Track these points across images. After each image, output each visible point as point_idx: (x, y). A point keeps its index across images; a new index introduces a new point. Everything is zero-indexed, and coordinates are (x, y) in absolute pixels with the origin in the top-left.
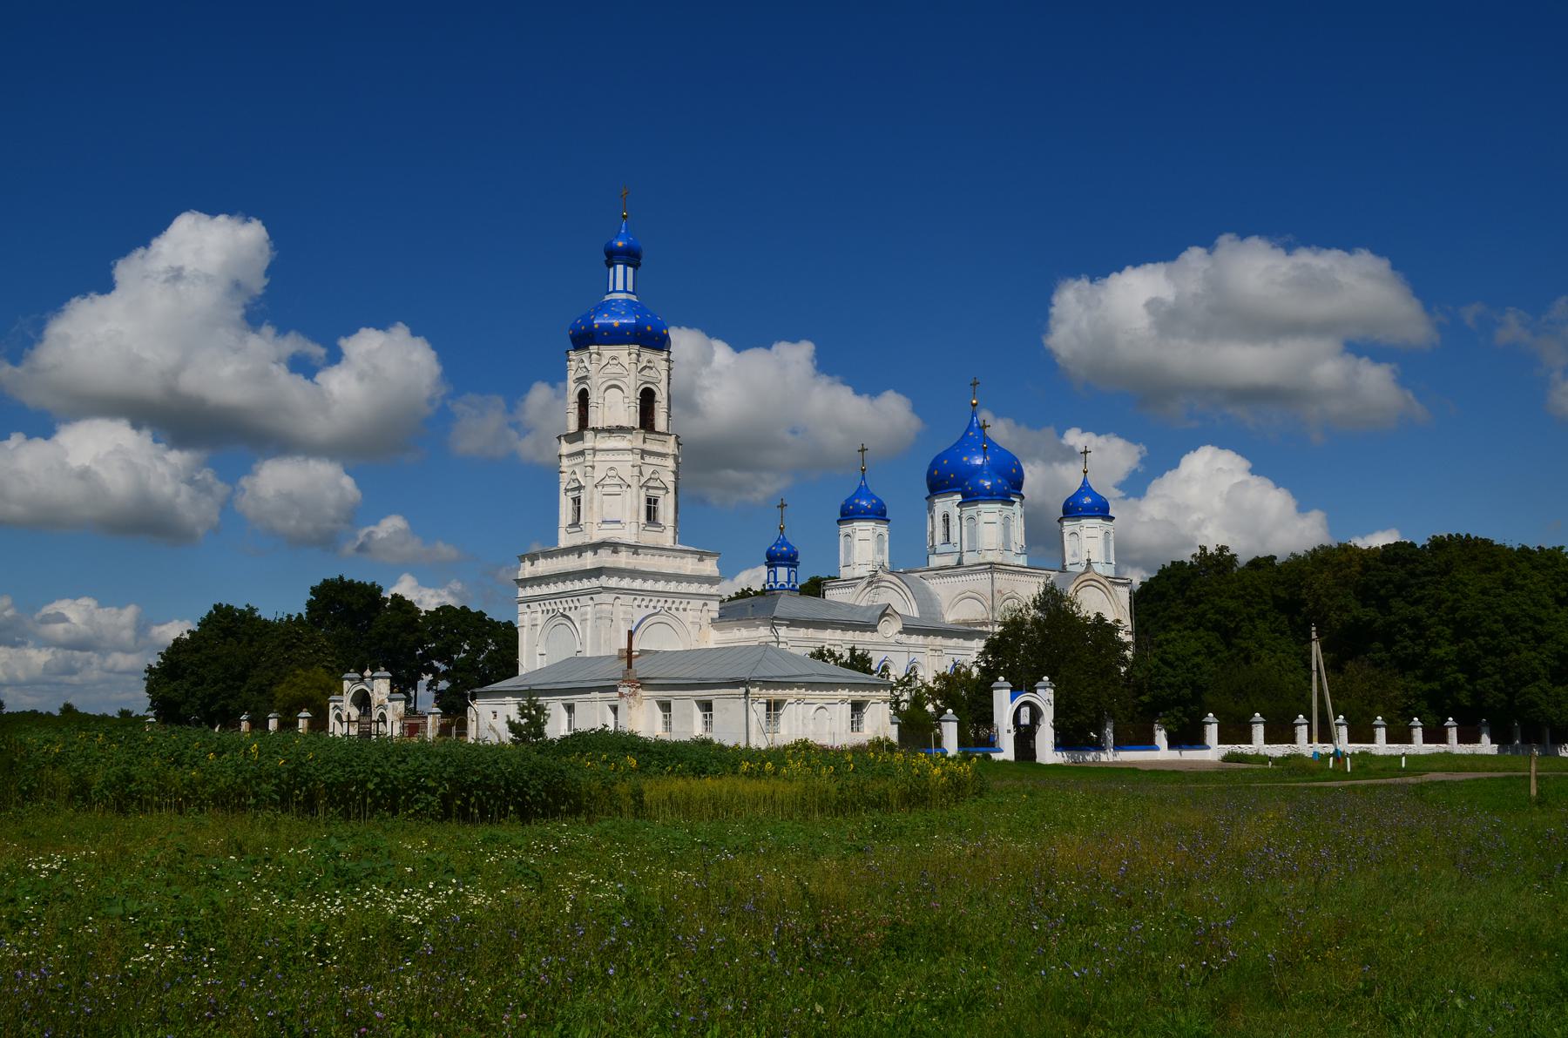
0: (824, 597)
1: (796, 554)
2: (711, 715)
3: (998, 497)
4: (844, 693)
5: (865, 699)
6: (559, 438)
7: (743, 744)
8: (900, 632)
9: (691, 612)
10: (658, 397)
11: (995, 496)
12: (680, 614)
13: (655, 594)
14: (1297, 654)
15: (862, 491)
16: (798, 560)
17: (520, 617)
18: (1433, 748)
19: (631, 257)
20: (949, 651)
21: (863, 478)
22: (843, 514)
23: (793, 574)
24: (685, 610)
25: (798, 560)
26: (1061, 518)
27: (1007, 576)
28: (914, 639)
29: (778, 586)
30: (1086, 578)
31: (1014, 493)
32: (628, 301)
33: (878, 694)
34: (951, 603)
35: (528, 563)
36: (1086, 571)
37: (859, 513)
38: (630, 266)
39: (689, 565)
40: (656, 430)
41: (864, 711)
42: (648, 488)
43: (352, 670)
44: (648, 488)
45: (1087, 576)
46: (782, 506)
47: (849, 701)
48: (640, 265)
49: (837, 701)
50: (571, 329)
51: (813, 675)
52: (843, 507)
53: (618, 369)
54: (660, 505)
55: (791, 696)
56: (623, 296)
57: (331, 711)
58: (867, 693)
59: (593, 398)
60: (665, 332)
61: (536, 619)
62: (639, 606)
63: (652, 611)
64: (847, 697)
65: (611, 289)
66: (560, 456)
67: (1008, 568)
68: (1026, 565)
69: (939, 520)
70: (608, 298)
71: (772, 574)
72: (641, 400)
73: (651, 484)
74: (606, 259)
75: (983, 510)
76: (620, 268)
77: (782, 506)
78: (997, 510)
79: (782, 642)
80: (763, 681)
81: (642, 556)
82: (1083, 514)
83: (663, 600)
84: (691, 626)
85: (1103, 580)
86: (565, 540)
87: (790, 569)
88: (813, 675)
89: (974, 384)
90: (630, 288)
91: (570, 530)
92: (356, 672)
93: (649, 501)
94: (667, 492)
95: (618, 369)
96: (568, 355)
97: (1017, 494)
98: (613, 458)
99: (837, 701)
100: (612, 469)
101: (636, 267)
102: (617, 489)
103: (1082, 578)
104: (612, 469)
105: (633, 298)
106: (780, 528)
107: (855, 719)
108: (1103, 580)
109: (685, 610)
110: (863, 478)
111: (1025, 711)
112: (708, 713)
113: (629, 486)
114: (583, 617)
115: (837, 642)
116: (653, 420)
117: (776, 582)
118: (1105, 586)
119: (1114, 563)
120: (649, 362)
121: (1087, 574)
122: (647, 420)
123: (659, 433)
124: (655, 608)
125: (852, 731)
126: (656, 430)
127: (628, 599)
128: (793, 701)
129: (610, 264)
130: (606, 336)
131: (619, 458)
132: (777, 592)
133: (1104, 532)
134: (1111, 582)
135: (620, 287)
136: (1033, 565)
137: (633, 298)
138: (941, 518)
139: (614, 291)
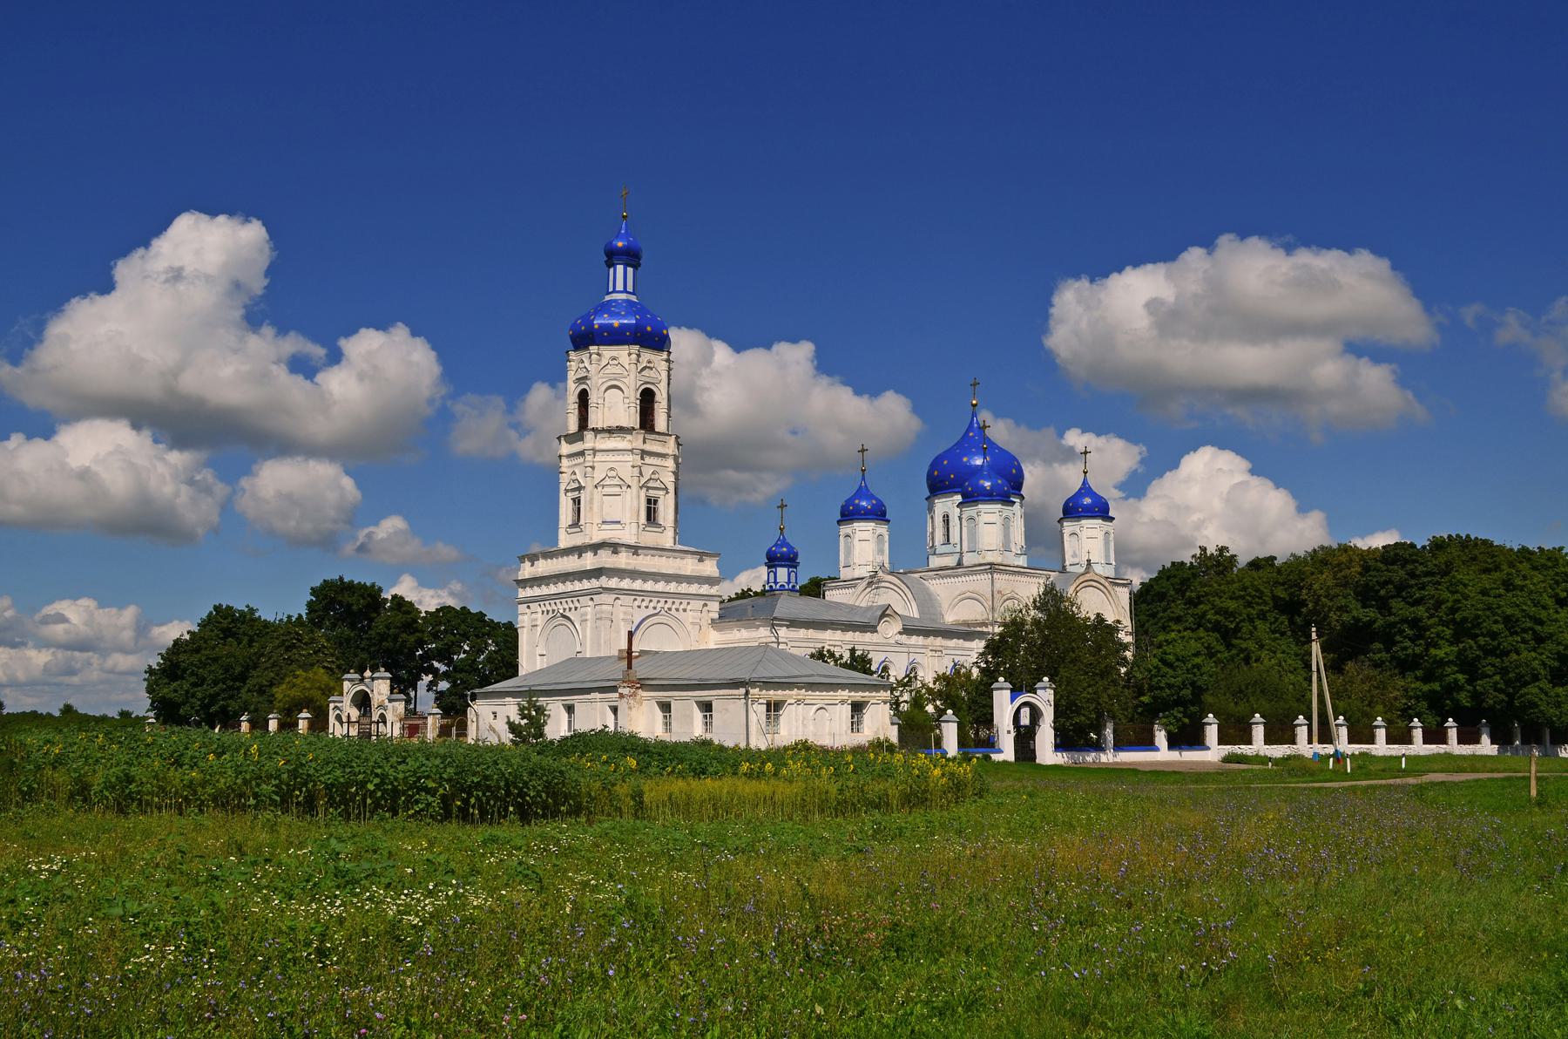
1: (796, 555)
2: (711, 716)
5: (863, 699)
6: (559, 438)
7: (743, 745)
9: (691, 613)
10: (658, 398)
12: (680, 615)
15: (862, 492)
17: (520, 617)
19: (631, 257)
20: (949, 652)
22: (843, 514)
24: (685, 610)
26: (1061, 519)
29: (778, 587)
30: (1086, 579)
32: (628, 301)
33: (879, 694)
35: (528, 564)
36: (1086, 572)
39: (689, 566)
40: (656, 430)
41: (864, 711)
43: (352, 671)
44: (648, 488)
45: (1087, 577)
47: (849, 702)
48: (640, 265)
49: (837, 702)
53: (618, 370)
54: (661, 505)
55: (791, 697)
56: (623, 296)
57: (331, 712)
59: (593, 398)
60: (665, 332)
61: (536, 620)
62: (639, 607)
63: (651, 611)
64: (847, 698)
65: (611, 289)
66: (560, 456)
68: (1026, 566)
70: (608, 298)
73: (651, 484)
76: (620, 268)
77: (782, 507)
78: (997, 511)
80: (763, 682)
82: (1083, 514)
83: (663, 600)
85: (1103, 581)
87: (791, 570)
90: (630, 289)
93: (649, 501)
94: (667, 493)
95: (618, 370)
98: (613, 459)
99: (837, 702)
100: (612, 469)
101: (635, 267)
102: (617, 490)
103: (1082, 579)
105: (633, 298)
108: (1103, 581)
110: (863, 479)
111: (1025, 712)
112: (708, 714)
113: (629, 486)
116: (653, 420)
117: (776, 583)
118: (1105, 587)
119: (1114, 563)
121: (1088, 575)
122: (647, 422)
123: (659, 433)
124: (655, 608)
125: (852, 732)
126: (656, 430)
127: (628, 599)
129: (610, 264)
130: (604, 336)
131: (618, 458)
132: (777, 592)
134: (1111, 582)
135: (620, 287)
137: (633, 298)
139: (614, 291)
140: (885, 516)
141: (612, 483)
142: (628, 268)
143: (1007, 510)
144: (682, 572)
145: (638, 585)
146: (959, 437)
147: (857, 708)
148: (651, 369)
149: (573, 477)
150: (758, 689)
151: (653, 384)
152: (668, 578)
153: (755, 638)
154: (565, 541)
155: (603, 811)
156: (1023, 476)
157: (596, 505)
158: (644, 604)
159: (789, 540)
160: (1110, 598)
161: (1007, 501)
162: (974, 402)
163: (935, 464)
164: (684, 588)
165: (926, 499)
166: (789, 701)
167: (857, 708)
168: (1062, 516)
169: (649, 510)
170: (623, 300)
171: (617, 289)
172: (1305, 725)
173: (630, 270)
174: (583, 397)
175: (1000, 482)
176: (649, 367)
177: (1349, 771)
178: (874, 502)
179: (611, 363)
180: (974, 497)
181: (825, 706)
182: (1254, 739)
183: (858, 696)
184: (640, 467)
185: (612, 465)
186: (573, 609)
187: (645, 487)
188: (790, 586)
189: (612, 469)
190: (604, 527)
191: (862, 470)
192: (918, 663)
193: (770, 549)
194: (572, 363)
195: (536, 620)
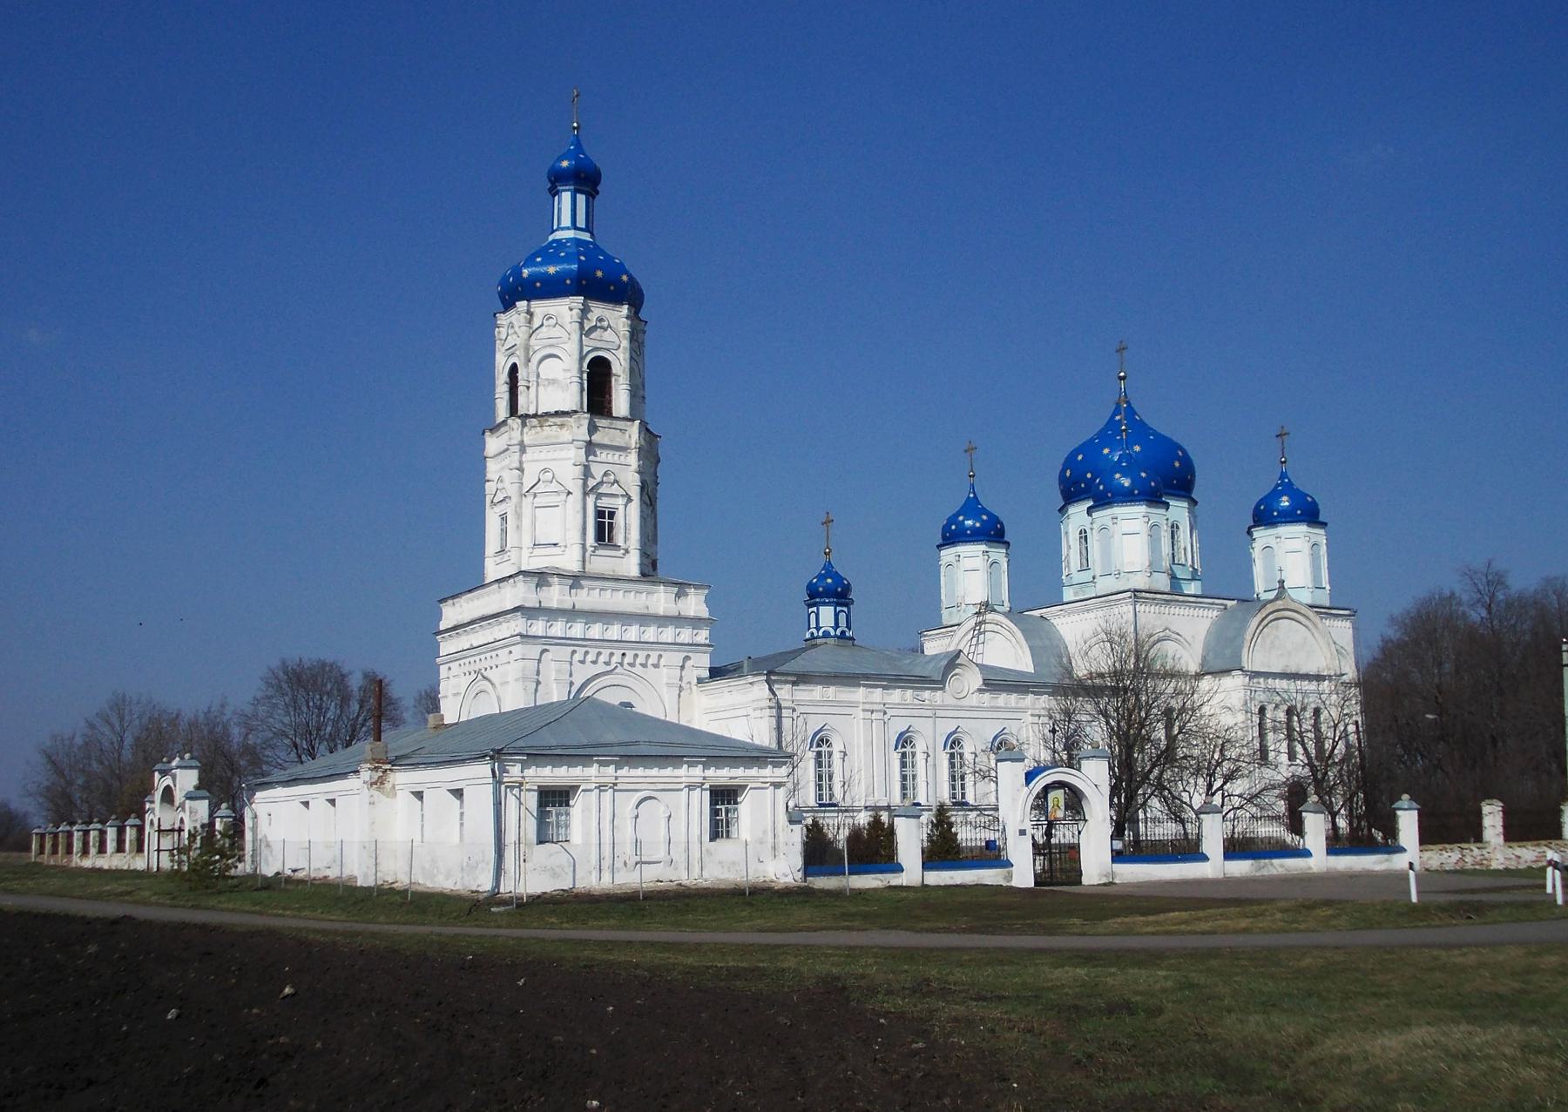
1: (847, 588)
4: (697, 772)
5: (735, 782)
8: (980, 690)
9: (665, 670)
14: (530, 430)
15: (972, 506)
18: (1446, 857)
19: (586, 180)
22: (944, 537)
23: (842, 617)
24: (656, 666)
26: (1250, 528)
28: (1003, 699)
29: (821, 634)
30: (1277, 608)
32: (578, 242)
36: (1277, 598)
38: (581, 192)
39: (661, 600)
45: (1279, 604)
46: (828, 522)
47: (707, 786)
49: (682, 786)
50: (500, 284)
54: (619, 519)
55: (587, 780)
56: (571, 234)
58: (739, 772)
62: (582, 662)
63: (601, 668)
64: (701, 780)
65: (555, 227)
67: (1159, 596)
69: (1074, 537)
70: (551, 238)
73: (602, 490)
76: (566, 197)
77: (828, 522)
78: (1140, 515)
80: (528, 754)
81: (586, 590)
82: (1279, 520)
83: (618, 653)
84: (665, 689)
85: (1305, 610)
87: (839, 609)
89: (1121, 350)
90: (581, 223)
91: (498, 559)
93: (600, 514)
94: (630, 500)
98: (550, 455)
99: (682, 786)
100: (545, 470)
101: (591, 195)
103: (1270, 608)
105: (586, 237)
106: (825, 553)
108: (1305, 610)
109: (656, 666)
111: (1057, 796)
117: (818, 628)
118: (1307, 618)
119: (1328, 587)
120: (600, 320)
121: (1279, 602)
123: (617, 418)
124: (607, 663)
132: (819, 641)
133: (1310, 544)
136: (1208, 593)
137: (586, 237)
138: (1078, 536)
140: (1003, 537)
142: (578, 196)
143: (1157, 514)
144: (652, 611)
146: (1102, 423)
147: (724, 796)
151: (608, 350)
154: (492, 570)
155: (1260, 869)
156: (600, 180)
157: (526, 522)
158: (590, 658)
159: (837, 568)
161: (1157, 502)
162: (1122, 374)
163: (1070, 461)
168: (1252, 524)
170: (568, 240)
171: (562, 226)
172: (1415, 809)
173: (581, 198)
176: (601, 328)
178: (985, 517)
183: (723, 775)
186: (489, 668)
188: (838, 633)
189: (545, 470)
190: (538, 551)
193: (811, 581)
194: (501, 329)
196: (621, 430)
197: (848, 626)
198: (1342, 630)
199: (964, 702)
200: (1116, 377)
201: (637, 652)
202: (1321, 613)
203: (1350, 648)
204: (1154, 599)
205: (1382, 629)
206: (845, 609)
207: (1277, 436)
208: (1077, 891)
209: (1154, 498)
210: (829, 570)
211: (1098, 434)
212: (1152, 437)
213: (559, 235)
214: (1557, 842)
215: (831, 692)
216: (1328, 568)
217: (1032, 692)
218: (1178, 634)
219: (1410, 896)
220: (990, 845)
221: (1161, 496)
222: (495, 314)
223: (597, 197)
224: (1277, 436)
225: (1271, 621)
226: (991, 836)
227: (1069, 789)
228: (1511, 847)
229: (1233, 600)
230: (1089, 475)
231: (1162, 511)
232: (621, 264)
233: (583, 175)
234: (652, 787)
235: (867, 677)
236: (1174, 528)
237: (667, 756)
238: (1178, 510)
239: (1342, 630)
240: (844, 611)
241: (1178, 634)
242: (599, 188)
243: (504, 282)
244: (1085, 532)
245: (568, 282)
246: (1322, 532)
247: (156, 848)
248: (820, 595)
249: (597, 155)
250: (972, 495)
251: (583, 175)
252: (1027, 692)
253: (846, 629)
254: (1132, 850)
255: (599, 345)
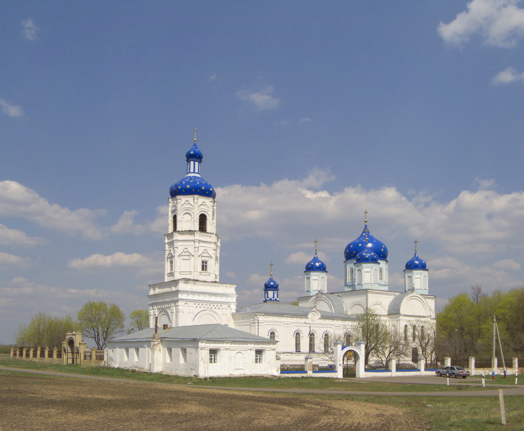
0: (298, 305)
1: (277, 286)
3: (371, 261)
4: (251, 346)
5: (262, 349)
6: (165, 235)
8: (320, 319)
10: (208, 218)
11: (370, 260)
12: (217, 311)
13: (227, 303)
16: (278, 288)
17: (150, 311)
21: (316, 254)
23: (276, 294)
24: (219, 309)
25: (278, 288)
26: (404, 270)
27: (374, 295)
28: (328, 321)
31: (380, 259)
33: (247, 346)
34: (350, 307)
35: (152, 290)
37: (313, 269)
40: (207, 232)
41: (263, 353)
42: (202, 256)
43: (69, 332)
44: (202, 256)
47: (254, 349)
48: (202, 161)
51: (235, 338)
52: (306, 266)
53: (189, 206)
57: (62, 348)
59: (178, 218)
60: (211, 189)
61: (155, 312)
63: (202, 309)
65: (188, 172)
66: (165, 243)
68: (388, 290)
70: (187, 176)
71: (266, 294)
72: (199, 219)
74: (186, 159)
75: (415, 273)
79: (261, 323)
80: (207, 340)
86: (167, 279)
87: (275, 292)
88: (235, 338)
90: (197, 171)
92: (80, 332)
93: (203, 262)
95: (189, 206)
96: (169, 200)
97: (385, 260)
98: (186, 244)
100: (186, 248)
101: (200, 162)
102: (188, 257)
104: (186, 248)
105: (198, 175)
107: (258, 357)
110: (316, 254)
113: (193, 256)
114: (172, 311)
115: (339, 325)
116: (206, 228)
117: (268, 297)
119: (428, 289)
122: (203, 227)
125: (257, 362)
127: (191, 304)
128: (223, 349)
129: (188, 161)
131: (188, 244)
134: (423, 297)
135: (192, 170)
137: (198, 175)
139: (190, 173)
141: (186, 254)
145: (196, 297)
147: (259, 352)
148: (204, 205)
149: (170, 252)
150: (204, 343)
152: (216, 295)
153: (282, 322)
160: (423, 304)
164: (218, 299)
165: (344, 262)
166: (221, 349)
167: (259, 352)
169: (203, 266)
171: (191, 172)
174: (175, 217)
175: (372, 254)
177: (428, 405)
179: (186, 203)
180: (361, 261)
181: (241, 351)
182: (478, 369)
184: (198, 247)
185: (186, 247)
187: (201, 256)
191: (315, 250)
192: (300, 331)
195: (155, 312)
196: (209, 237)
197: (277, 297)
198: (431, 303)
199: (315, 322)
200: (364, 221)
201: (218, 304)
202: (425, 297)
203: (434, 310)
204: (374, 292)
205: (445, 302)
206: (277, 292)
207: (414, 242)
208: (180, 354)
209: (374, 261)
210: (271, 280)
211: (357, 239)
212: (375, 241)
213: (190, 175)
214: (490, 368)
215: (276, 319)
216: (428, 283)
217: (336, 320)
218: (381, 303)
219: (447, 383)
220: (331, 366)
221: (377, 261)
222: (168, 199)
223: (201, 163)
224: (414, 242)
225: (410, 299)
226: (332, 363)
227: (353, 352)
228: (476, 370)
229: (398, 293)
230: (354, 252)
231: (378, 265)
232: (210, 185)
233: (197, 156)
234: (239, 349)
235: (286, 314)
236: (381, 271)
237: (244, 341)
238: (382, 264)
239: (431, 303)
240: (276, 293)
241: (381, 303)
242: (202, 160)
243: (171, 188)
244: (352, 269)
245: (193, 190)
246: (427, 272)
247: (77, 359)
248: (270, 287)
249: (202, 149)
250: (316, 256)
251: (197, 156)
252: (335, 320)
253: (277, 298)
254: (369, 369)
255: (203, 210)
